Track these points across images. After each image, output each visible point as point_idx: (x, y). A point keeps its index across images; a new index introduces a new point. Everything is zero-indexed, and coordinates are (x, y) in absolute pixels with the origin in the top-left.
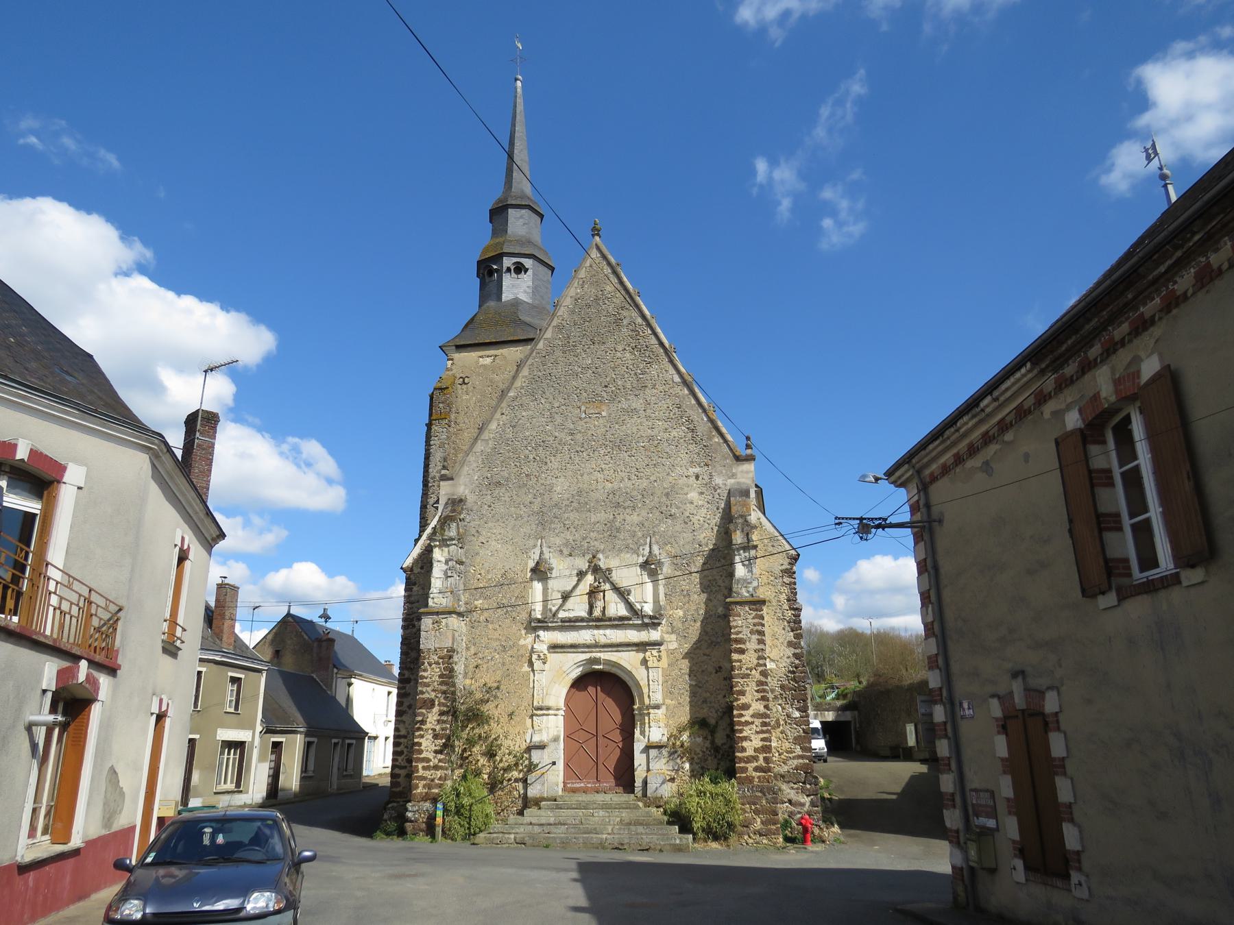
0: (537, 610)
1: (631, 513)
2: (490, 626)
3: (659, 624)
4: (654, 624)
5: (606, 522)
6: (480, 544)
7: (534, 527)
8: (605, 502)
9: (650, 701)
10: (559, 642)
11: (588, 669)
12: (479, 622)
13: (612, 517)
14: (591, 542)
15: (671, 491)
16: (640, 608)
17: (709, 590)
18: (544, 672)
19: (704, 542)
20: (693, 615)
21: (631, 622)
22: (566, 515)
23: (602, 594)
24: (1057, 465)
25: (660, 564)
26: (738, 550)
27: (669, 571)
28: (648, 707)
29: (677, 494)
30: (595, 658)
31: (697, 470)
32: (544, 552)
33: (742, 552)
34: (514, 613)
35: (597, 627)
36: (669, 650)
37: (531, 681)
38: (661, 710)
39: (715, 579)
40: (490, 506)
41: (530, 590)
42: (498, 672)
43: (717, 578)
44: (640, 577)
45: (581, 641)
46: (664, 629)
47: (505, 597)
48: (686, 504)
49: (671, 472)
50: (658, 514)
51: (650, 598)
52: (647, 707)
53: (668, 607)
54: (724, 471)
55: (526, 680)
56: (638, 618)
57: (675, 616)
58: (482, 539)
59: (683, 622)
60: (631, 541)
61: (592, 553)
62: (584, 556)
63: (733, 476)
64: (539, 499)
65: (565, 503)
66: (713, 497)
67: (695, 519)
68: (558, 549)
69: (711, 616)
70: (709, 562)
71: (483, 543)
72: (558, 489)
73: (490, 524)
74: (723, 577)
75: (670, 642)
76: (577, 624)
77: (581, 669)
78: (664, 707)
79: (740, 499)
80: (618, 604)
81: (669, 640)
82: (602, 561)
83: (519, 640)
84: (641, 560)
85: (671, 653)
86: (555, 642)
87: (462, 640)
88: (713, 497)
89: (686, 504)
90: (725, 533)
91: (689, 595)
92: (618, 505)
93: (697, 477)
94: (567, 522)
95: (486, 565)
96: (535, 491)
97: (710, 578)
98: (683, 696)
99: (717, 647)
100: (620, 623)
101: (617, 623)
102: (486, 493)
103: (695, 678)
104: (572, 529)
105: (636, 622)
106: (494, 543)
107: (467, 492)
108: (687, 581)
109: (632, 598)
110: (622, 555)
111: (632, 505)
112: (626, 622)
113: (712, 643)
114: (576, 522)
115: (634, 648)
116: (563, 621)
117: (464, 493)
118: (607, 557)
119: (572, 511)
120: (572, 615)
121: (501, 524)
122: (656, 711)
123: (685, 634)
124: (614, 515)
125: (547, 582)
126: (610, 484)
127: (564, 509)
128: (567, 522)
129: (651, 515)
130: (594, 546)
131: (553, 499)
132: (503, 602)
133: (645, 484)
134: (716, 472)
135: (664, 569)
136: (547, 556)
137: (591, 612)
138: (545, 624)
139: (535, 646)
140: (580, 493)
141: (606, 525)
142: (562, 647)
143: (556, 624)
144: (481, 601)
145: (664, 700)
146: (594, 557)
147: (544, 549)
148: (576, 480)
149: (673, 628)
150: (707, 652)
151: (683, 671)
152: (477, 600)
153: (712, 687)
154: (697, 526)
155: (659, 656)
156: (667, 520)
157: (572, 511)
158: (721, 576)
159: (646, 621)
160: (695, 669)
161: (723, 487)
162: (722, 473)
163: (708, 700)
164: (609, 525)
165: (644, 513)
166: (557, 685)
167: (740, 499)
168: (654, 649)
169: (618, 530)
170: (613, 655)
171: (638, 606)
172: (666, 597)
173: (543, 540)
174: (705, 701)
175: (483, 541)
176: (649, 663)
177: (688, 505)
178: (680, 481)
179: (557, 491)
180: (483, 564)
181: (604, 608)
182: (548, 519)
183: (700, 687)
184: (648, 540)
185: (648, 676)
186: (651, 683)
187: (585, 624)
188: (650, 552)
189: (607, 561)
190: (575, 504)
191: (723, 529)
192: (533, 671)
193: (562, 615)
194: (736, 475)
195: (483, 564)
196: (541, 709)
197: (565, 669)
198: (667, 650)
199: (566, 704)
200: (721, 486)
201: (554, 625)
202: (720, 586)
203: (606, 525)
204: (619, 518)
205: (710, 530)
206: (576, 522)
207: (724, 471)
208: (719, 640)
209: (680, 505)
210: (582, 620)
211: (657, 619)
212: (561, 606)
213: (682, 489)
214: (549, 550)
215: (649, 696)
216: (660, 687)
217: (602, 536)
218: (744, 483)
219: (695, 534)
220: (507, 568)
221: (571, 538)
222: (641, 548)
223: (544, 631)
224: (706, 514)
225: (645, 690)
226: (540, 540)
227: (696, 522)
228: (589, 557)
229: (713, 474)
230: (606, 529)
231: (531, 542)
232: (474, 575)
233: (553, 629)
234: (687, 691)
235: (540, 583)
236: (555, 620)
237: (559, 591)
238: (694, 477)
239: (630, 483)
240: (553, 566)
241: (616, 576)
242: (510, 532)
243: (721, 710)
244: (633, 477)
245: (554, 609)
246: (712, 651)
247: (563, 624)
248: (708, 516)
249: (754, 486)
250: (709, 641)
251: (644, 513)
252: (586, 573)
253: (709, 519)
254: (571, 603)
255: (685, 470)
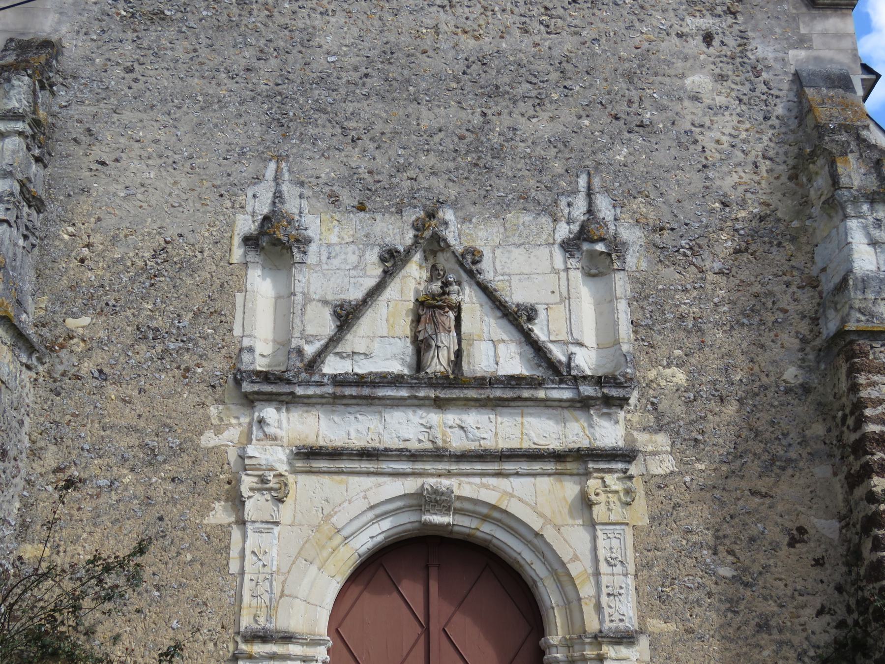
0: (258, 351)
1: (531, 112)
2: (112, 391)
3: (623, 402)
4: (609, 402)
5: (464, 132)
6: (95, 166)
7: (257, 130)
8: (458, 82)
9: (601, 621)
10: (322, 443)
11: (406, 521)
12: (77, 377)
13: (477, 120)
14: (421, 177)
15: (639, 66)
16: (564, 359)
17: (756, 320)
18: (276, 530)
19: (733, 195)
20: (714, 382)
21: (541, 394)
22: (350, 107)
23: (452, 315)
24: (508, 510)
25: (617, 248)
26: (855, 201)
27: (644, 265)
28: (599, 638)
29: (656, 74)
30: (436, 492)
31: (707, 22)
32: (286, 195)
33: (865, 207)
34: (186, 357)
35: (439, 404)
36: (653, 476)
37: (234, 552)
38: (637, 648)
39: (770, 294)
40: (130, 70)
41: (239, 297)
42: (128, 524)
43: (778, 289)
44: (563, 275)
45: (390, 441)
46: (635, 418)
47: (163, 312)
48: (680, 99)
49: (637, 24)
50: (606, 119)
51: (588, 332)
52: (595, 637)
53: (644, 360)
54: (778, 30)
55: (219, 551)
56: (561, 381)
57: (663, 383)
58: (98, 152)
59: (688, 402)
60: (532, 183)
61: (425, 206)
62: (400, 212)
63: (803, 42)
64: (273, 62)
65: (345, 77)
66: (753, 90)
67: (707, 139)
68: (327, 189)
69: (766, 388)
70: (753, 247)
71: (103, 163)
72: (329, 41)
73: (128, 116)
74: (793, 288)
75: (654, 453)
76: (381, 392)
77: (386, 524)
78: (644, 642)
79: (831, 93)
80: (501, 347)
81: (650, 448)
82: (452, 228)
83: (201, 434)
84: (563, 231)
85: (661, 483)
86: (311, 441)
87: (21, 423)
88: (753, 90)
89: (680, 99)
90: (790, 178)
91: (700, 330)
92: (495, 92)
93: (708, 38)
94: (352, 124)
95: (109, 222)
96: (262, 42)
97: (757, 288)
98: (697, 610)
99: (790, 471)
100: (509, 394)
101: (498, 393)
102: (121, 35)
103: (730, 558)
104: (366, 142)
105: (555, 394)
106: (134, 165)
107: (64, 29)
108: (695, 293)
109: (539, 331)
110: (509, 216)
111: (533, 93)
112: (526, 394)
113: (774, 459)
114: (379, 127)
115: (550, 467)
116: (339, 381)
117: (56, 31)
118: (466, 219)
119: (367, 96)
120: (363, 367)
121: (161, 118)
122: (623, 651)
123: (695, 435)
124: (484, 115)
125: (290, 275)
126: (472, 42)
127: (343, 91)
128: (352, 124)
129: (587, 122)
130: (429, 189)
131: (314, 66)
132: (154, 324)
133: (569, 46)
134: (754, 30)
135: (629, 258)
136: (291, 206)
137: (419, 365)
138: (286, 389)
139: (251, 451)
140: (389, 54)
141: (461, 138)
142: (335, 454)
143: (318, 391)
144: (85, 320)
145: (642, 618)
146: (431, 215)
147: (285, 188)
148: (377, 23)
149: (659, 418)
150: (761, 485)
151: (694, 538)
152: (75, 316)
153: (781, 584)
154: (713, 156)
155: (628, 492)
156: (633, 136)
157: (367, 96)
158: (788, 285)
159: (587, 390)
160: (729, 531)
161: (778, 66)
162: (773, 33)
163: (773, 623)
164: (470, 137)
165: (567, 115)
166: (313, 569)
167: (831, 93)
168: (610, 471)
169: (497, 153)
170: (486, 487)
171: (558, 354)
172: (635, 332)
173: (284, 165)
174: (763, 626)
175: (104, 158)
176: (595, 509)
177: (687, 103)
178: (663, 44)
179: (325, 47)
180: (99, 219)
181: (459, 354)
182: (299, 113)
183: (746, 585)
184: (582, 182)
185: (595, 549)
186: (604, 568)
187: (404, 393)
188: (590, 211)
189: (467, 228)
190: (375, 82)
191: (783, 167)
192: (242, 523)
193: (332, 366)
194: (811, 40)
195: (99, 219)
196: (264, 637)
197: (339, 520)
198: (647, 478)
199: (335, 628)
200: (771, 63)
201: (310, 391)
202: (785, 311)
203: (461, 138)
204: (500, 125)
205: (749, 168)
206: (379, 127)
207: (778, 30)
208: (793, 454)
209: (665, 101)
210: (396, 381)
211: (619, 385)
212: (334, 341)
213: (670, 64)
214: (297, 190)
215: (598, 607)
216: (630, 580)
217: (451, 165)
218: (831, 61)
219: (710, 175)
220: (171, 232)
221: (363, 166)
222: (563, 202)
223: (278, 410)
224: (736, 129)
225: (587, 590)
226: (272, 165)
227: (710, 146)
228: (413, 215)
229: (750, 34)
230: (462, 148)
231: (248, 169)
232: (69, 249)
233: (307, 402)
234: (710, 595)
235: (268, 280)
236: (316, 378)
237: (325, 302)
238: (699, 38)
239: (527, 40)
240: (310, 233)
241: (488, 270)
242: (187, 139)
243: (812, 653)
244: (535, 26)
245: (310, 350)
246: (776, 483)
247: (339, 391)
248: (744, 135)
249: (859, 69)
250: (766, 457)
251: (567, 115)
252: (409, 252)
253: (744, 141)
254: (356, 340)
255: (674, 20)
